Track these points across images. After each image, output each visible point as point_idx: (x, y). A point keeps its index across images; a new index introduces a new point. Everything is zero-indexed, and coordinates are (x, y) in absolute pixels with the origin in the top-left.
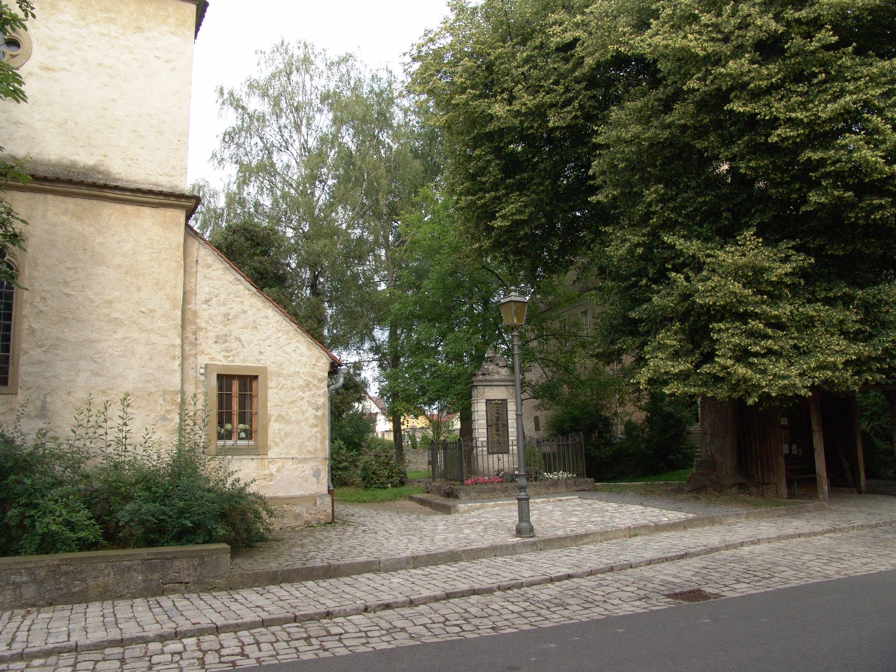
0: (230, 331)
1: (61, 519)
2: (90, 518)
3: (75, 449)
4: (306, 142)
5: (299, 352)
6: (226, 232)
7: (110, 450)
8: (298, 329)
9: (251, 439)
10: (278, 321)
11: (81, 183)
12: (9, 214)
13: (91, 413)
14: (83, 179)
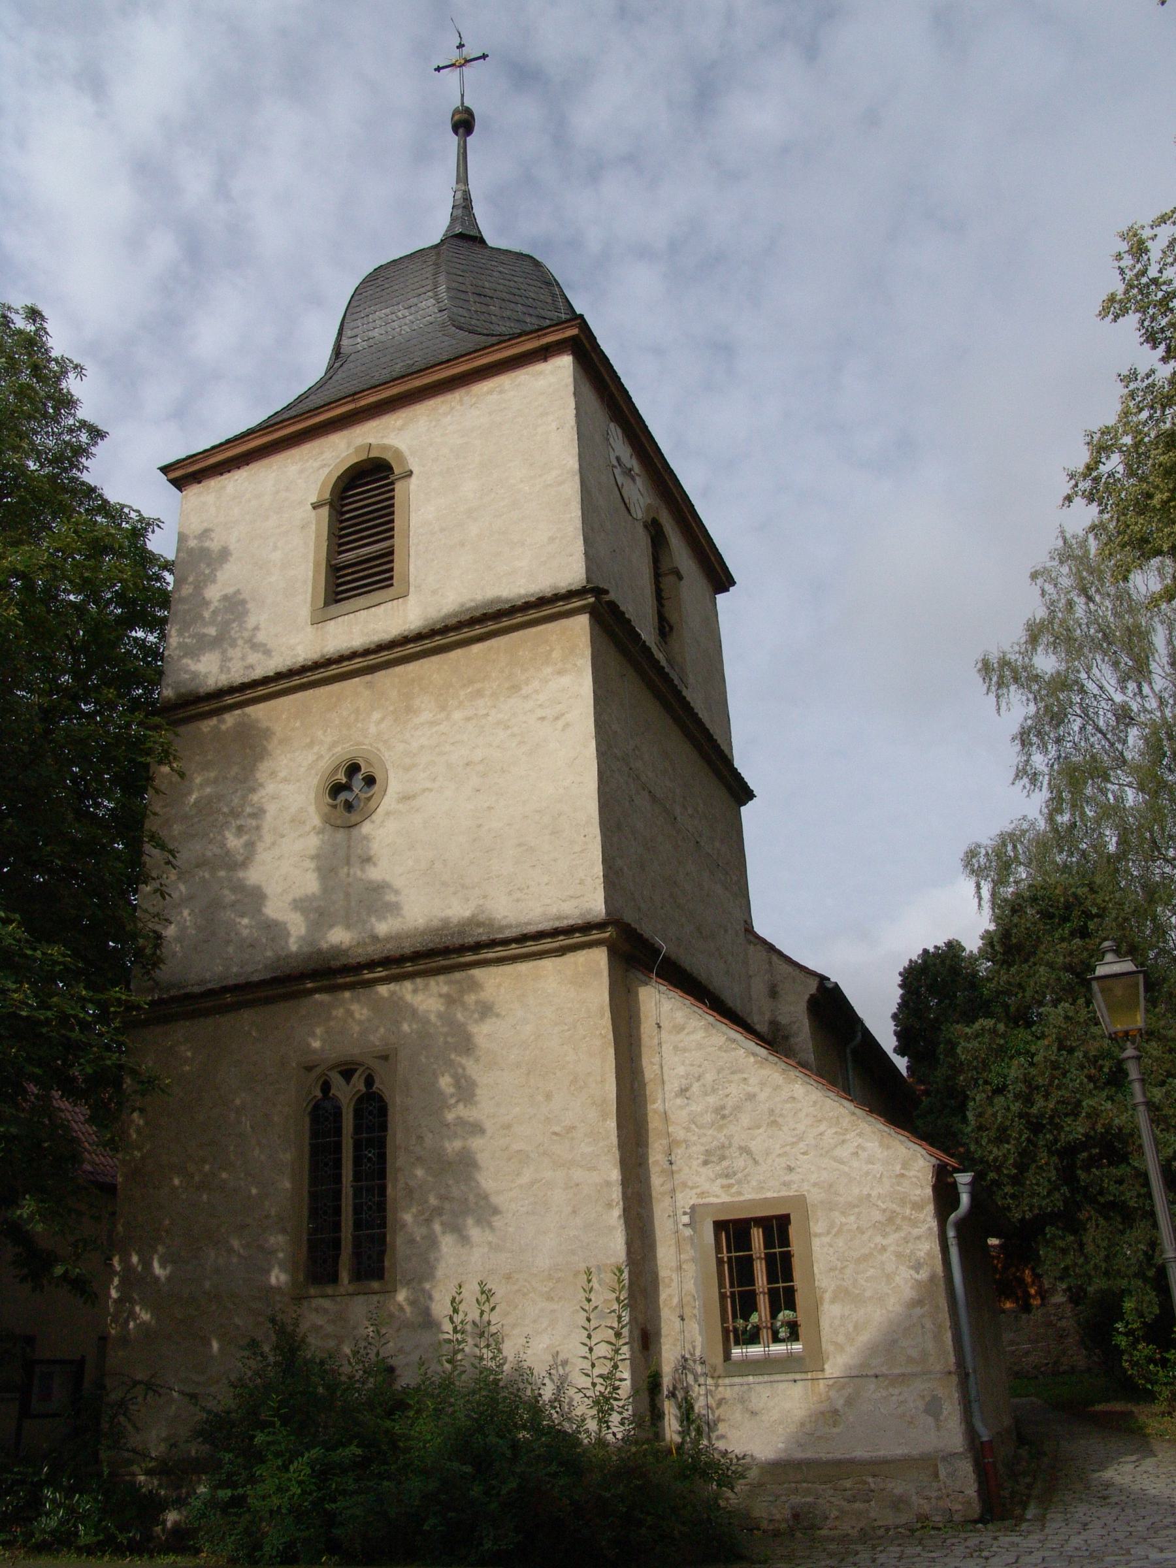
0: (730, 1138)
5: (863, 1155)
8: (858, 1111)
9: (797, 1339)
10: (815, 1103)
14: (461, 942)
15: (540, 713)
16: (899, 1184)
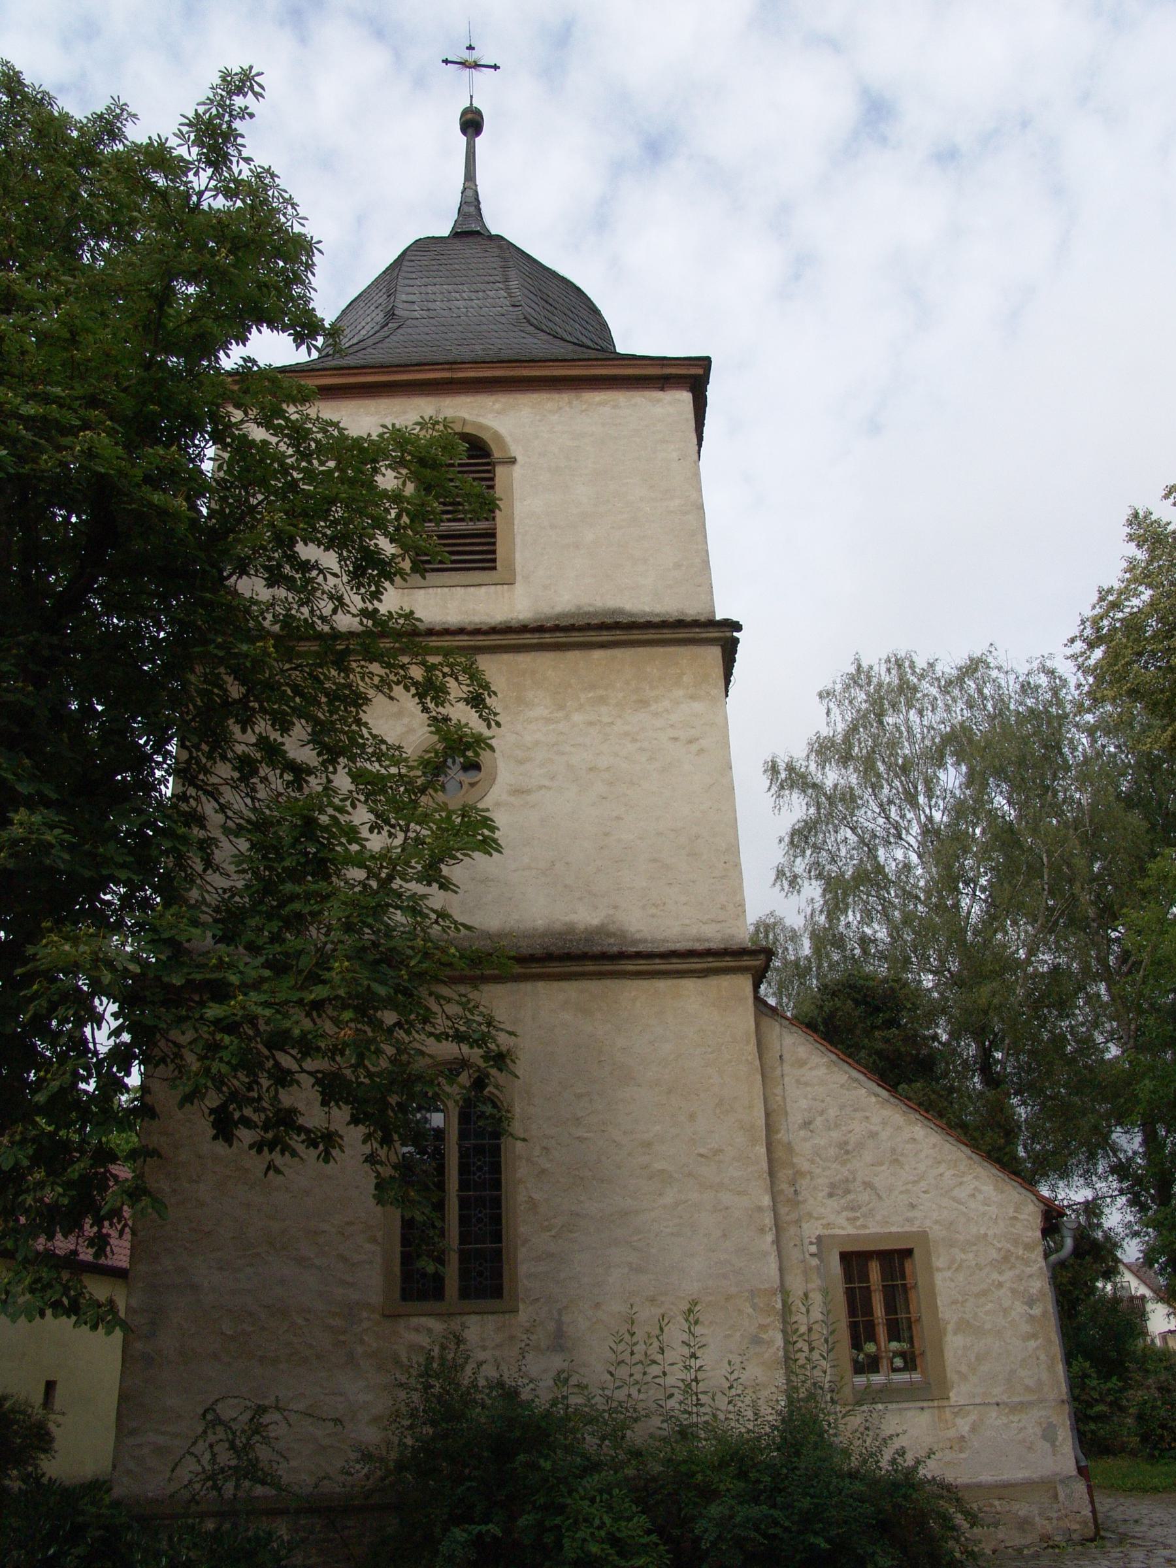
1: (603, 1533)
2: (649, 1532)
3: (614, 1405)
4: (930, 819)
5: (980, 1197)
6: (819, 996)
7: (672, 1403)
8: (974, 1156)
10: (934, 1146)
11: (584, 957)
12: (489, 1024)
13: (635, 1339)
14: (586, 949)
15: (672, 733)
16: (1013, 1226)
